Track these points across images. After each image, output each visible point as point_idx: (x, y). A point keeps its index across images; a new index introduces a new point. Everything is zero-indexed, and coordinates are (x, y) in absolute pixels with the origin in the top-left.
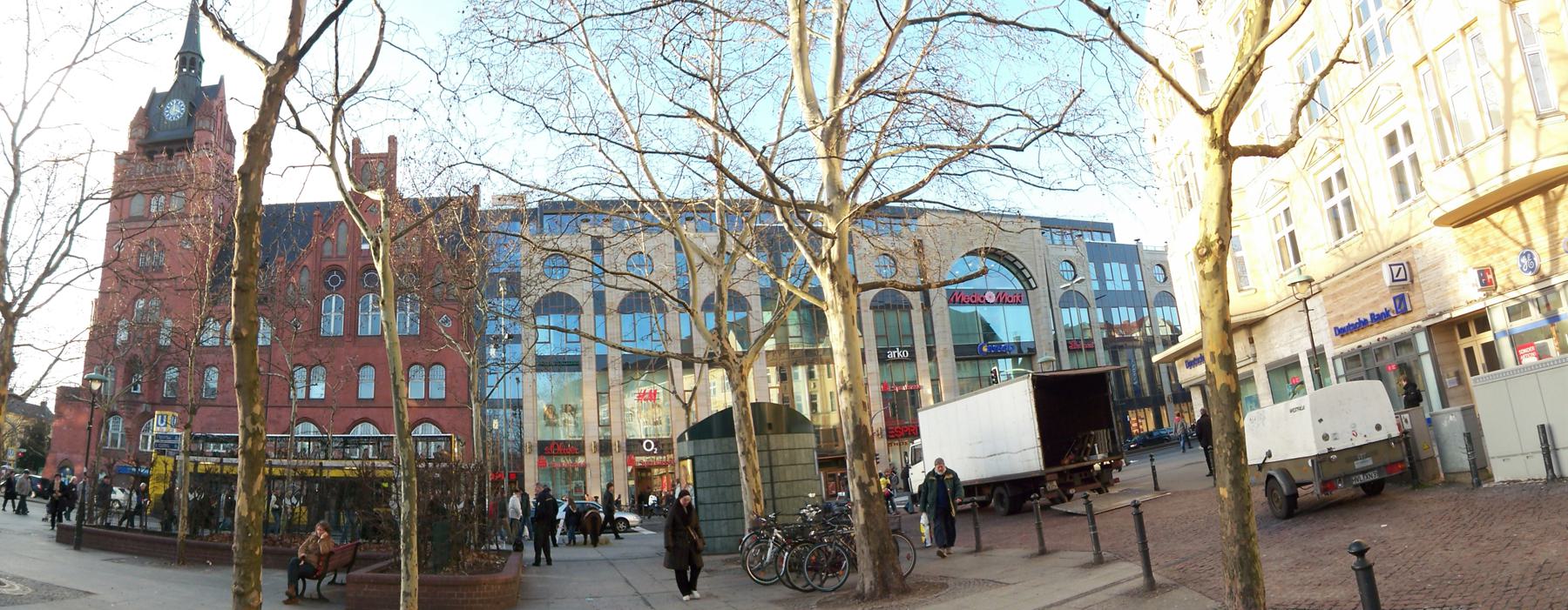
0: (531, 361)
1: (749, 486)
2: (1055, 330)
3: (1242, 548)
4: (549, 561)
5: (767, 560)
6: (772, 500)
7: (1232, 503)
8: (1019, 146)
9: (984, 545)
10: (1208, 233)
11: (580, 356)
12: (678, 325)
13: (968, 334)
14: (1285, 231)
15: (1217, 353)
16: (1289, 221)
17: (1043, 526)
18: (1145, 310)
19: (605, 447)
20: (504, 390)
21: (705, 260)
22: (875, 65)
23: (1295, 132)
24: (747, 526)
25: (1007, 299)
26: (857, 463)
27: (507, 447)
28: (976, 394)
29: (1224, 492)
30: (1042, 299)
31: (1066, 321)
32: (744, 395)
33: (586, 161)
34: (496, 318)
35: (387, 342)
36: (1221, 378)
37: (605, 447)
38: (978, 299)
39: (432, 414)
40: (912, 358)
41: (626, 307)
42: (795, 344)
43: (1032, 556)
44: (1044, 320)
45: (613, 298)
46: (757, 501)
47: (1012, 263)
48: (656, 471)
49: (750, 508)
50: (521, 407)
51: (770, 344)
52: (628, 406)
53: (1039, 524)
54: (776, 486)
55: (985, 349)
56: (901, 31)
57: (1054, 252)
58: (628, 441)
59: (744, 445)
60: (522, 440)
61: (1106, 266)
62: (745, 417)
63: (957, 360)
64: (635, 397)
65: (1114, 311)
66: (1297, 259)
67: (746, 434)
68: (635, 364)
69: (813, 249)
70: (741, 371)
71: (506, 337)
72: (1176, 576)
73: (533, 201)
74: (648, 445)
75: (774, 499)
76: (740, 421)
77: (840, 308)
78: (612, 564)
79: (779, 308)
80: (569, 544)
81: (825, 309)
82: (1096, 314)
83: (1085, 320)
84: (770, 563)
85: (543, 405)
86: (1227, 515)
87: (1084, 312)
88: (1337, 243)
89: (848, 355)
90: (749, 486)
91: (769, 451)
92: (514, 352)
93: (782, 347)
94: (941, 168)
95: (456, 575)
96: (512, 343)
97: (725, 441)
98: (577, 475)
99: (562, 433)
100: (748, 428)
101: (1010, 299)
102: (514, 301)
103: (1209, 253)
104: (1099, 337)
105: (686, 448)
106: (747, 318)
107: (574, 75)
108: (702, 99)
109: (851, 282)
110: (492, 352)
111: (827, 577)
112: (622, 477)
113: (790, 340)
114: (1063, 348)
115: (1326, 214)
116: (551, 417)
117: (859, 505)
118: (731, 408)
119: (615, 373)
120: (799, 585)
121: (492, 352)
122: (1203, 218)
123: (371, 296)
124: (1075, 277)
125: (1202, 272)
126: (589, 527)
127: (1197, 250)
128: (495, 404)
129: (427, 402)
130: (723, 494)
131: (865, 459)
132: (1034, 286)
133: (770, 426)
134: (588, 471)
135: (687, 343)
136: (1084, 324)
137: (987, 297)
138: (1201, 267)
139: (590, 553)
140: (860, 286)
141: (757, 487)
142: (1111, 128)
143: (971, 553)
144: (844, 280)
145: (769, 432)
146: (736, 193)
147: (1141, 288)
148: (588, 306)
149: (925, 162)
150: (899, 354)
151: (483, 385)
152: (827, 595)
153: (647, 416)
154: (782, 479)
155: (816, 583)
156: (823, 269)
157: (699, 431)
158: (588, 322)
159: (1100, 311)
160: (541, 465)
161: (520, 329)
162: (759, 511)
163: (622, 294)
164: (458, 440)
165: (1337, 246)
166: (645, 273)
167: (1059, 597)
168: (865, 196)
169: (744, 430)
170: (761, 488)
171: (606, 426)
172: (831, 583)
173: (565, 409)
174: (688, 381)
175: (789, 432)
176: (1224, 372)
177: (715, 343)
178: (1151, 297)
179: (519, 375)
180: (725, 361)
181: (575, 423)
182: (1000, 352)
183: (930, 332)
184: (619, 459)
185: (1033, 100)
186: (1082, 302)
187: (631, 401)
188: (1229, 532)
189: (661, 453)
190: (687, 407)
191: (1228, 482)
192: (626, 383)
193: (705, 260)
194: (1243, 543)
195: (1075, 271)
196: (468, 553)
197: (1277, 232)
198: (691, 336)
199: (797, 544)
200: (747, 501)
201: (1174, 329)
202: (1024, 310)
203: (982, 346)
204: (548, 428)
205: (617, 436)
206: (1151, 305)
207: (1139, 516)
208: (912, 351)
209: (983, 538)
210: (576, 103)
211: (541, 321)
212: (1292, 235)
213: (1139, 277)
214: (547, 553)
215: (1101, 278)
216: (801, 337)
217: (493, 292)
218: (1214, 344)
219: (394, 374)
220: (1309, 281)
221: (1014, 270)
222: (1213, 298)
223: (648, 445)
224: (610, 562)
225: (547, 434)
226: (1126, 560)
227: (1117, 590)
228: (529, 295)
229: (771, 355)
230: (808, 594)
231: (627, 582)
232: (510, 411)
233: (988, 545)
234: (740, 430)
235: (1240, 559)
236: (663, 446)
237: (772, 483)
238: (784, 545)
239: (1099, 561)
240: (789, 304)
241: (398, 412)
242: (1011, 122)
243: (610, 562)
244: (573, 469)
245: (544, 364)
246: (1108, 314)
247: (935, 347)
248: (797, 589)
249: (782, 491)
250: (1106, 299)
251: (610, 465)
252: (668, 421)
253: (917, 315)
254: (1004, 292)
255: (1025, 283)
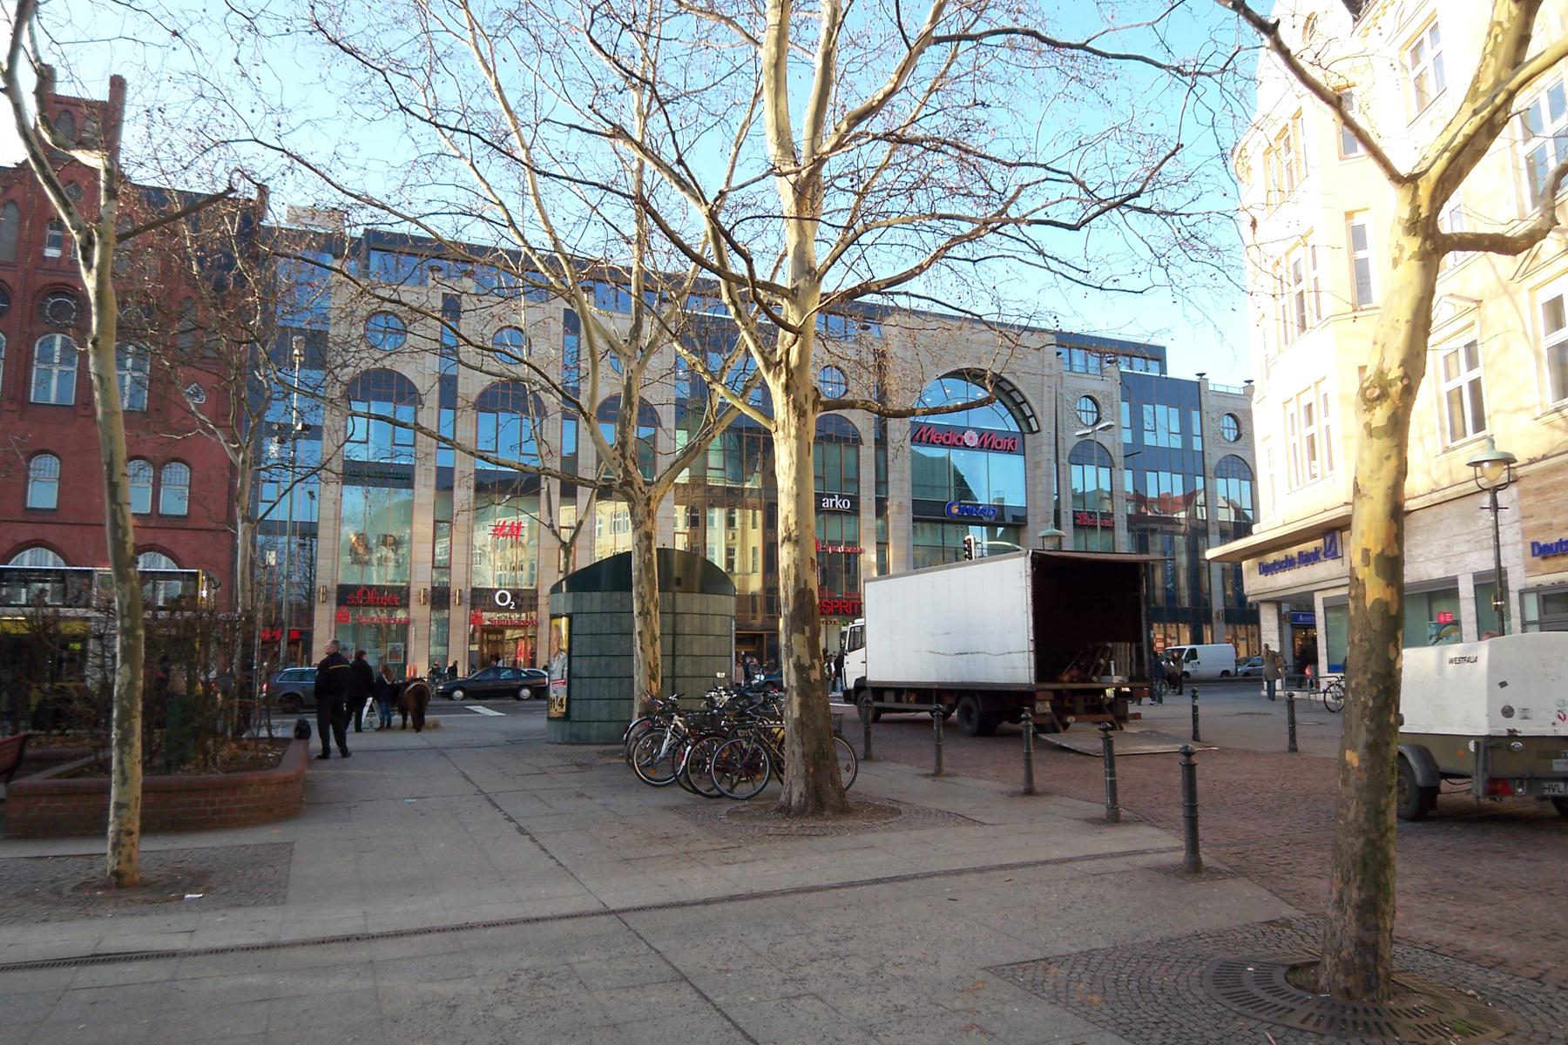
0: (337, 466)
1: (645, 656)
2: (1058, 494)
3: (1369, 842)
4: (345, 752)
5: (662, 755)
6: (672, 680)
7: (1364, 776)
8: (1074, 223)
9: (946, 769)
10: (1386, 366)
11: (412, 467)
12: (560, 435)
13: (934, 487)
14: (1464, 379)
15: (1375, 550)
16: (1472, 362)
17: (1033, 757)
18: (1200, 480)
19: (439, 598)
20: (293, 508)
21: (612, 346)
22: (880, 96)
23: (1548, 215)
24: (637, 710)
25: (994, 444)
26: (796, 637)
27: (288, 594)
28: (948, 568)
29: (1352, 758)
30: (1045, 449)
31: (1077, 484)
32: (649, 536)
33: (448, 178)
34: (287, 395)
35: (99, 410)
36: (1375, 590)
37: (439, 598)
38: (953, 439)
39: (163, 539)
40: (855, 511)
41: (487, 402)
42: (715, 479)
43: (1013, 795)
44: (1044, 479)
45: (471, 385)
46: (653, 677)
47: (1018, 405)
48: (508, 633)
49: (643, 686)
50: (315, 535)
51: (683, 477)
52: (478, 542)
53: (1028, 754)
54: (679, 661)
55: (955, 510)
56: (921, 51)
57: (1071, 382)
58: (474, 589)
59: (643, 603)
60: (312, 583)
61: (1147, 408)
62: (648, 566)
63: (914, 520)
64: (490, 530)
65: (1151, 476)
66: (1479, 424)
67: (647, 588)
68: (493, 484)
69: (766, 340)
70: (648, 504)
71: (299, 427)
72: (1232, 860)
73: (359, 223)
74: (503, 597)
75: (674, 677)
76: (640, 571)
77: (793, 432)
78: (443, 754)
79: (706, 425)
80: (381, 728)
81: (773, 430)
82: (1122, 477)
83: (1105, 485)
84: (664, 759)
85: (349, 534)
86: (1352, 791)
87: (1105, 473)
88: (1558, 404)
89: (798, 495)
90: (644, 658)
91: (674, 614)
92: (308, 451)
93: (698, 481)
94: (947, 248)
95: (204, 775)
96: (307, 438)
97: (617, 595)
98: (393, 635)
99: (375, 575)
100: (651, 581)
101: (999, 443)
102: (317, 375)
103: (1383, 396)
104: (1122, 511)
105: (564, 601)
106: (655, 436)
107: (440, 49)
108: (628, 107)
109: (811, 397)
110: (273, 448)
111: (739, 781)
112: (461, 638)
113: (709, 473)
114: (1067, 520)
115: (1545, 354)
116: (361, 550)
117: (795, 694)
118: (627, 556)
119: (463, 494)
120: (702, 789)
121: (273, 448)
122: (1380, 340)
123: (58, 339)
124: (1098, 421)
125: (1368, 425)
126: (412, 704)
127: (1363, 391)
128: (272, 528)
129: (154, 520)
130: (608, 665)
131: (808, 634)
132: (1035, 428)
133: (679, 581)
134: (412, 629)
135: (571, 461)
136: (1102, 490)
137: (966, 438)
138: (1368, 417)
139: (411, 739)
140: (822, 403)
141: (655, 659)
142: (1211, 202)
143: (927, 776)
144: (802, 392)
145: (677, 588)
146: (666, 260)
147: (1197, 446)
148: (432, 399)
149: (928, 237)
150: (837, 503)
151: (256, 499)
152: (739, 804)
153: (503, 558)
154: (687, 652)
155: (724, 788)
156: (777, 376)
157: (582, 581)
158: (429, 416)
159: (1128, 475)
160: (340, 619)
161: (328, 419)
162: (655, 691)
163: (487, 380)
164: (209, 579)
165: (1558, 410)
166: (524, 354)
167: (1057, 854)
168: (835, 281)
169: (645, 583)
170: (659, 662)
171: (446, 568)
172: (744, 789)
173: (384, 541)
174: (566, 515)
175: (703, 591)
176: (1381, 582)
177: (616, 463)
178: (1211, 462)
179: (315, 488)
180: (628, 489)
181: (397, 562)
182: (973, 515)
183: (883, 478)
184: (458, 614)
185: (1091, 158)
186: (1105, 459)
187: (483, 535)
188: (1351, 816)
189: (518, 609)
190: (567, 548)
191: (1361, 745)
192: (479, 512)
193: (612, 346)
194: (1373, 836)
195: (1098, 412)
196: (223, 743)
197: (1448, 378)
198: (576, 454)
199: (703, 737)
200: (640, 678)
201: (1239, 512)
202: (1016, 461)
203: (951, 505)
204: (356, 566)
205: (458, 582)
206: (1209, 473)
207: (1190, 769)
208: (855, 501)
209: (945, 760)
210: (438, 87)
211: (359, 407)
212: (1475, 386)
213: (1196, 430)
214: (341, 741)
215: (1137, 425)
216: (724, 469)
217: (280, 356)
218: (1372, 536)
219: (110, 464)
220: (1507, 460)
221: (1009, 404)
222: (1380, 466)
223: (503, 597)
224: (441, 752)
225: (352, 577)
226: (1152, 825)
227: (1141, 861)
228: (345, 365)
229: (680, 491)
230: (711, 801)
231: (466, 777)
232: (296, 540)
233: (951, 770)
234: (639, 583)
235: (1363, 858)
236: (524, 600)
237: (674, 656)
238: (685, 738)
239: (1114, 818)
240: (720, 420)
241: (116, 526)
242: (1054, 190)
243: (441, 752)
244: (389, 626)
245: (356, 474)
246: (1139, 481)
247: (886, 499)
248: (701, 794)
249: (685, 667)
250: (1140, 458)
251: (445, 624)
252: (532, 567)
253: (868, 452)
254: (991, 433)
255: (1023, 424)
